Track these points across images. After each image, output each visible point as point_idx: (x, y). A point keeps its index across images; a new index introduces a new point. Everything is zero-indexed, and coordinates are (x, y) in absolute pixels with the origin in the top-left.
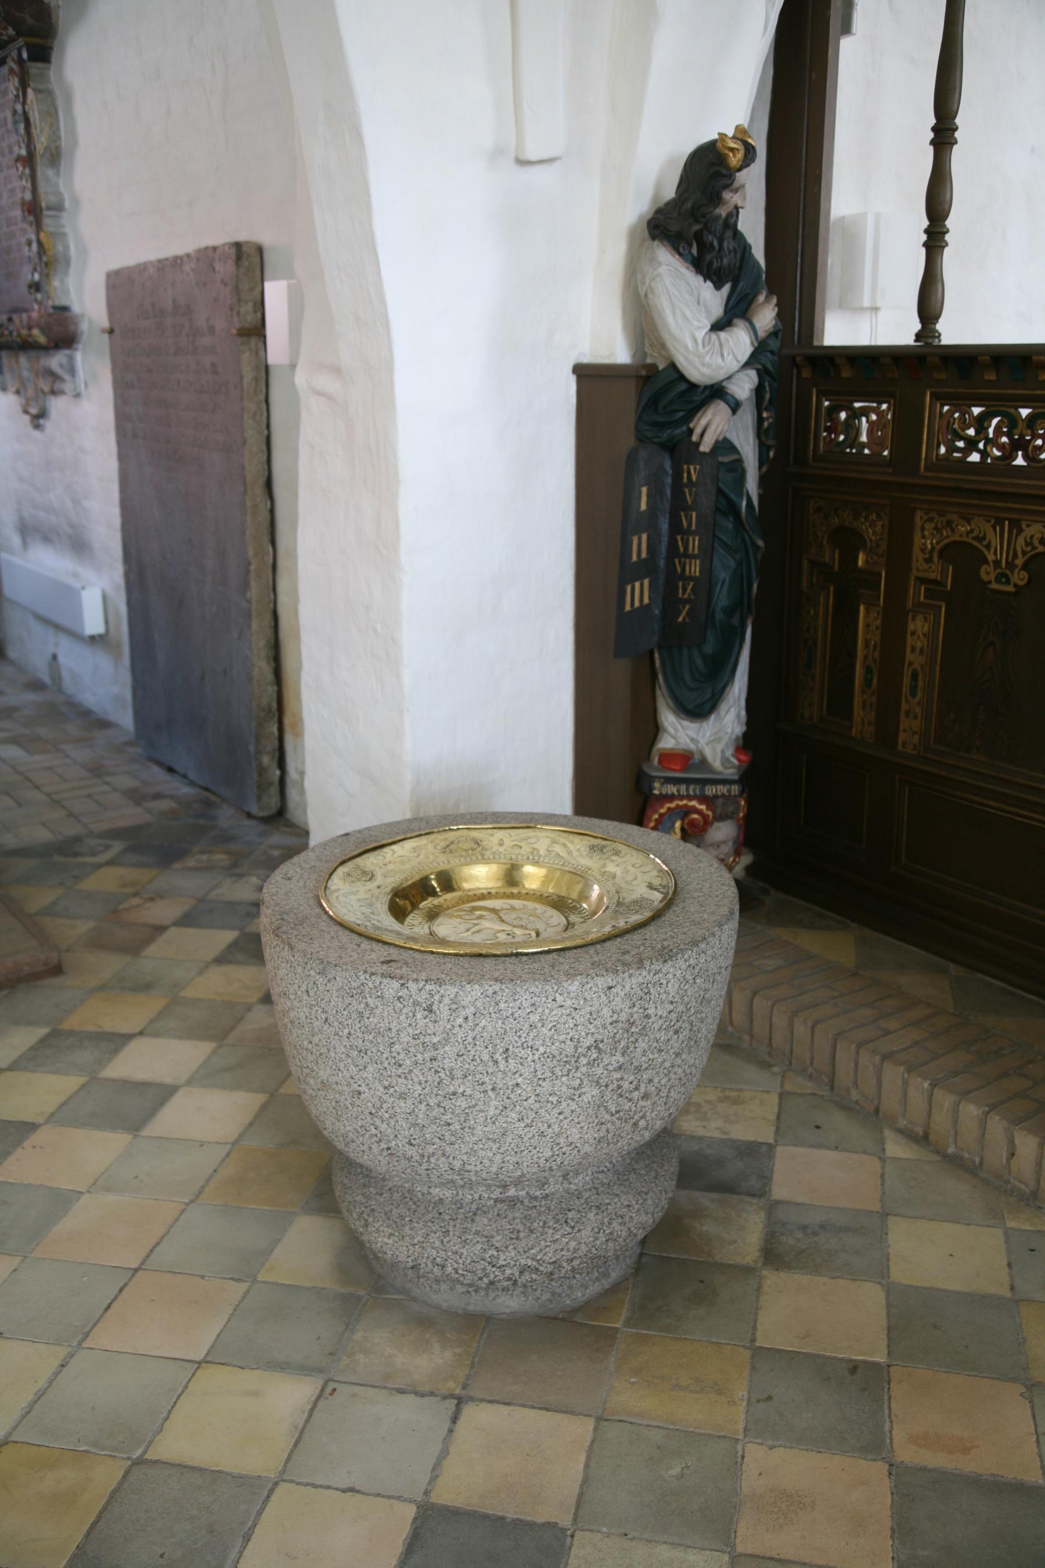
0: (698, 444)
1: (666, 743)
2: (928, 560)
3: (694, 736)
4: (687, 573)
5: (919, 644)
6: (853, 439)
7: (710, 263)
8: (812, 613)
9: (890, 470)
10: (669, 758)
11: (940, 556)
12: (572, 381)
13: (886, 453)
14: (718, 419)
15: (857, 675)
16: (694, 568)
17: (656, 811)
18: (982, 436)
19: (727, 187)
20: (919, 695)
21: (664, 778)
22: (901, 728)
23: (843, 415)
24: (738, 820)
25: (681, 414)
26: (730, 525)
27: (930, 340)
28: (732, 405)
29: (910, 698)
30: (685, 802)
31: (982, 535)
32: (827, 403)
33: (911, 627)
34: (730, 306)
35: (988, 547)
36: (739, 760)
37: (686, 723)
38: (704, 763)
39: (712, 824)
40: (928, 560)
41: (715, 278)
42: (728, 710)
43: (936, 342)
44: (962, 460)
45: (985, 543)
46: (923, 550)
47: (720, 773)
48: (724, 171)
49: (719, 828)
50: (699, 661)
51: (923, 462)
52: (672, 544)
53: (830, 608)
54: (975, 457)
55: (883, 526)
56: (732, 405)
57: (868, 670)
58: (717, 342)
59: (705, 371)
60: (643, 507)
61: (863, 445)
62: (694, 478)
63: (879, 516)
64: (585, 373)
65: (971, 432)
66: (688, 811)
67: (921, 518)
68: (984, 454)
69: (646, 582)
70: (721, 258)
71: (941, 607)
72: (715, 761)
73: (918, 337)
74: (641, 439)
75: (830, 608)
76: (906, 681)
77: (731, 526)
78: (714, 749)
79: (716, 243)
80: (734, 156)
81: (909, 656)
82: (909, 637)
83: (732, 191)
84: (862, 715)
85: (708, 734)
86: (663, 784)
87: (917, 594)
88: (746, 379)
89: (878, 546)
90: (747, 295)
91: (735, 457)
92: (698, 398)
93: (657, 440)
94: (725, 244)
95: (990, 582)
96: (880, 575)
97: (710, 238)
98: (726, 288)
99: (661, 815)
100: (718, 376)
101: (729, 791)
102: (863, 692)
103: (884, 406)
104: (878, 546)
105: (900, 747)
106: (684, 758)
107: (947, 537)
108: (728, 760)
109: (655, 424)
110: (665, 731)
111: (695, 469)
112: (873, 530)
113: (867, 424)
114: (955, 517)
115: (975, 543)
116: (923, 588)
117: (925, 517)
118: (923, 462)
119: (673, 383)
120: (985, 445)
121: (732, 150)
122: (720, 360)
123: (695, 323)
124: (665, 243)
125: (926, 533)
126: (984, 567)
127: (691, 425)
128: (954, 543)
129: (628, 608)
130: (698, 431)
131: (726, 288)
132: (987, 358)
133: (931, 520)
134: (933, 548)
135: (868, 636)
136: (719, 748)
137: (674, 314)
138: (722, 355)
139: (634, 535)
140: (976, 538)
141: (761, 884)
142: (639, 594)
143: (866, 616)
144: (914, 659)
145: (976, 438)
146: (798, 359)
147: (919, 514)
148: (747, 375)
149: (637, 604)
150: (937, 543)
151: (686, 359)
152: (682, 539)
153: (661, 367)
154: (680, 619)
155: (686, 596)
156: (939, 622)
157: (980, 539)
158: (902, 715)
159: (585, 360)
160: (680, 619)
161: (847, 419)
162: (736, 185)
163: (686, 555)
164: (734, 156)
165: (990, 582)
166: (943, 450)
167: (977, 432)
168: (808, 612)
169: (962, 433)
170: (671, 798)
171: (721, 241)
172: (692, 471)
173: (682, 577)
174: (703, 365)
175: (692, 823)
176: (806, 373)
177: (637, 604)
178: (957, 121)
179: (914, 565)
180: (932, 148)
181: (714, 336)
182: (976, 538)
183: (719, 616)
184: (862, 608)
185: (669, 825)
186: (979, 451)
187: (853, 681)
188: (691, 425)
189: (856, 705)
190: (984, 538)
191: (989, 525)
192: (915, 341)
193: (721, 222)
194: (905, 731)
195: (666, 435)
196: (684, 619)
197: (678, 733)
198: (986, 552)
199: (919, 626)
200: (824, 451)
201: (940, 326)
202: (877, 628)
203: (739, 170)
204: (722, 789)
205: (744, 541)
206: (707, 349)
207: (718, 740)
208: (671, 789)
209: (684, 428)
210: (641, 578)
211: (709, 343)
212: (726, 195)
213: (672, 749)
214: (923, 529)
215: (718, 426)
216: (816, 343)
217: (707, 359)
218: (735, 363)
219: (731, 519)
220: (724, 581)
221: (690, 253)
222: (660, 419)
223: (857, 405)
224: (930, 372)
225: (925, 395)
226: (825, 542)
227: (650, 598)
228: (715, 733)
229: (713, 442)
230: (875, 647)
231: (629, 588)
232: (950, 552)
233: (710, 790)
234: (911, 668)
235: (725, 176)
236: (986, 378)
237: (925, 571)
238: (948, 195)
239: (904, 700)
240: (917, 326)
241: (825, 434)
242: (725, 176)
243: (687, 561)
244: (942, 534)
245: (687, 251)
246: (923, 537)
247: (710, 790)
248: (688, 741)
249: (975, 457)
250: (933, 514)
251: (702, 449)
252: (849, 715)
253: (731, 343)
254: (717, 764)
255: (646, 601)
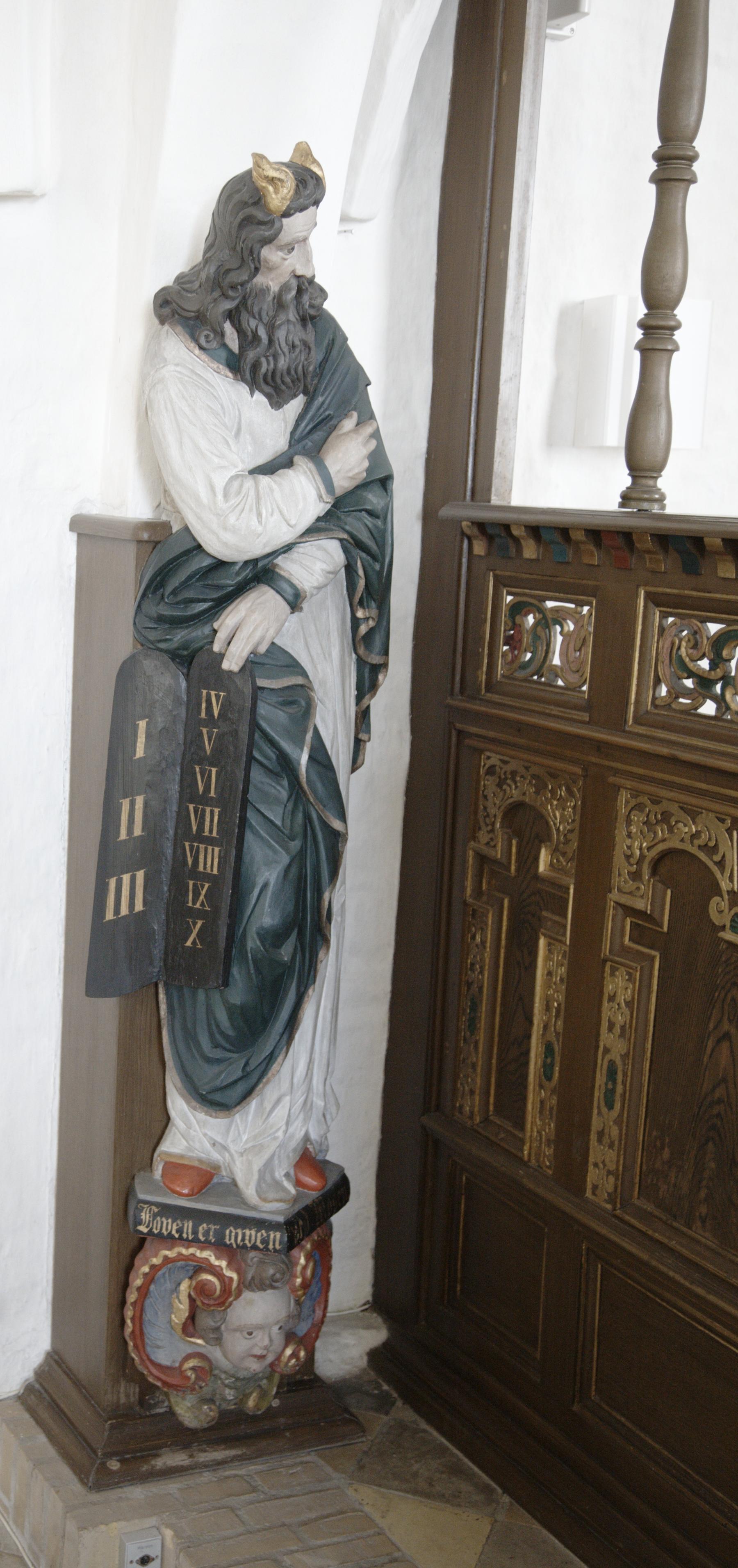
0: (222, 656)
1: (174, 1145)
2: (636, 876)
3: (219, 1139)
4: (201, 868)
5: (620, 1019)
6: (542, 664)
7: (256, 366)
8: (478, 938)
9: (586, 717)
10: (176, 1169)
11: (654, 871)
12: (70, 541)
13: (585, 688)
14: (256, 617)
15: (533, 1054)
16: (210, 860)
17: (146, 1261)
18: (719, 673)
19: (268, 241)
20: (618, 1105)
21: (157, 1204)
22: (591, 1160)
23: (531, 619)
24: (294, 1290)
25: (206, 605)
26: (282, 792)
27: (645, 505)
28: (291, 598)
29: (604, 1110)
30: (191, 1250)
31: (712, 844)
32: (509, 598)
33: (609, 988)
34: (297, 435)
35: (721, 864)
36: (298, 1183)
37: (202, 1116)
38: (232, 1188)
39: (239, 1294)
40: (636, 876)
41: (268, 389)
42: (278, 1101)
43: (656, 509)
44: (691, 712)
45: (717, 858)
46: (628, 857)
47: (254, 1208)
48: (260, 215)
49: (251, 1302)
50: (222, 1016)
51: (632, 708)
52: (182, 818)
53: (503, 936)
54: (709, 708)
55: (574, 808)
56: (291, 598)
57: (549, 1050)
58: (252, 493)
59: (228, 537)
60: (689, 701)
61: (555, 672)
62: (216, 713)
63: (569, 791)
64: (89, 532)
65: (705, 664)
66: (202, 1267)
67: (627, 802)
68: (720, 701)
69: (140, 875)
70: (275, 357)
71: (653, 959)
72: (248, 1185)
73: (626, 499)
74: (145, 644)
75: (503, 936)
76: (600, 1079)
77: (284, 794)
78: (250, 1163)
79: (262, 333)
80: (276, 191)
81: (606, 1038)
82: (605, 1004)
83: (280, 248)
84: (537, 1126)
85: (245, 1138)
86: (155, 1216)
87: (615, 931)
88: (319, 554)
89: (567, 842)
90: (329, 418)
91: (300, 680)
92: (230, 581)
93: (162, 646)
94: (281, 335)
95: (723, 928)
96: (568, 889)
97: (253, 323)
98: (296, 405)
99: (153, 1267)
100: (257, 549)
101: (265, 1241)
102: (541, 1086)
103: (586, 609)
104: (567, 842)
105: (589, 1194)
106: (205, 1178)
107: (664, 840)
108: (278, 1184)
109: (160, 619)
110: (174, 1125)
111: (218, 697)
112: (561, 815)
113: (563, 639)
114: (674, 808)
115: (702, 856)
116: (628, 921)
117: (633, 802)
118: (632, 708)
119: (187, 553)
120: (723, 689)
121: (272, 180)
122: (254, 521)
123: (216, 460)
124: (179, 329)
125: (634, 829)
126: (716, 899)
127: (216, 625)
128: (684, 852)
129: (110, 915)
130: (221, 637)
131: (296, 405)
132: (719, 541)
133: (639, 807)
134: (642, 857)
135: (551, 992)
136: (258, 1163)
137: (181, 445)
138: (259, 515)
139: (125, 797)
140: (703, 848)
141: (385, 1387)
142: (130, 893)
143: (547, 959)
144: (612, 1044)
145: (691, 674)
146: (464, 524)
147: (624, 796)
148: (320, 548)
149: (124, 911)
150: (649, 848)
151: (199, 518)
152: (196, 811)
153: (175, 529)
154: (189, 943)
155: (198, 906)
156: (650, 986)
157: (712, 850)
158: (593, 1137)
159: (95, 510)
160: (189, 943)
161: (536, 625)
162: (285, 237)
163: (200, 837)
164: (276, 191)
165: (723, 928)
166: (664, 690)
167: (714, 665)
168: (473, 937)
169: (691, 665)
170: (169, 1240)
171: (271, 328)
172: (214, 699)
173: (194, 873)
174: (225, 529)
175: (202, 1289)
176: (479, 548)
177: (124, 911)
178: (698, 144)
179: (616, 881)
180: (653, 188)
181: (249, 483)
182: (703, 848)
183: (253, 943)
184: (542, 942)
185: (169, 1286)
186: (715, 698)
187: (527, 1064)
188: (216, 625)
189: (530, 1107)
190: (715, 848)
191: (722, 828)
192: (622, 505)
193: (270, 298)
194: (596, 1165)
195: (179, 636)
196: (194, 942)
197: (192, 1132)
198: (718, 875)
199: (618, 986)
200: (503, 676)
201: (663, 483)
202: (562, 980)
203: (287, 214)
204: (253, 1235)
205: (307, 818)
206: (233, 501)
207: (258, 1149)
208: (169, 1226)
209: (207, 630)
210: (132, 869)
211: (239, 493)
212: (269, 254)
213: (182, 1157)
214: (629, 822)
215: (255, 629)
216: (495, 500)
217: (232, 520)
218: (285, 528)
219: (285, 783)
220: (265, 885)
221: (225, 346)
222: (167, 612)
223: (550, 604)
224: (643, 556)
225: (637, 596)
226: (498, 825)
227: (145, 902)
228: (255, 1137)
229: (245, 654)
230: (558, 1010)
231: (113, 883)
232: (666, 863)
233: (233, 1236)
234: (608, 1057)
235: (261, 223)
236: (721, 574)
237: (630, 893)
238: (679, 264)
239: (595, 1111)
240: (625, 481)
241: (505, 648)
242: (261, 223)
243: (202, 846)
244: (655, 833)
245: (214, 344)
246: (629, 835)
247: (233, 1236)
248: (208, 1145)
249: (709, 708)
250: (645, 799)
251: (225, 665)
252: (520, 1123)
253: (277, 495)
254: (250, 1192)
255: (139, 907)
